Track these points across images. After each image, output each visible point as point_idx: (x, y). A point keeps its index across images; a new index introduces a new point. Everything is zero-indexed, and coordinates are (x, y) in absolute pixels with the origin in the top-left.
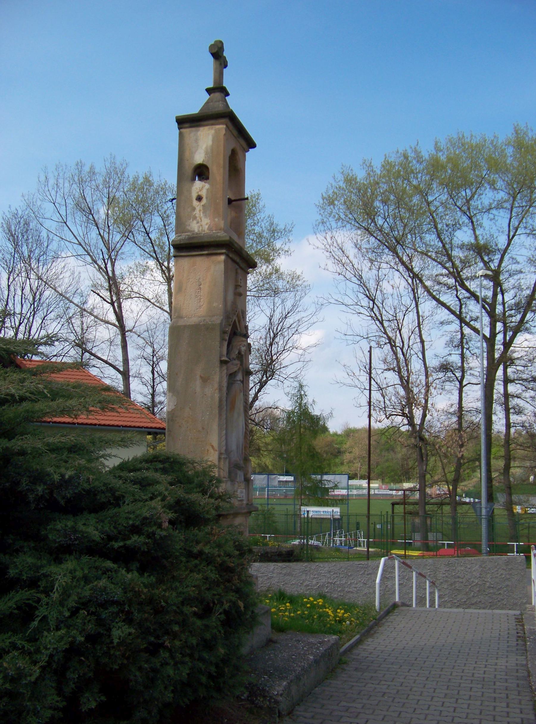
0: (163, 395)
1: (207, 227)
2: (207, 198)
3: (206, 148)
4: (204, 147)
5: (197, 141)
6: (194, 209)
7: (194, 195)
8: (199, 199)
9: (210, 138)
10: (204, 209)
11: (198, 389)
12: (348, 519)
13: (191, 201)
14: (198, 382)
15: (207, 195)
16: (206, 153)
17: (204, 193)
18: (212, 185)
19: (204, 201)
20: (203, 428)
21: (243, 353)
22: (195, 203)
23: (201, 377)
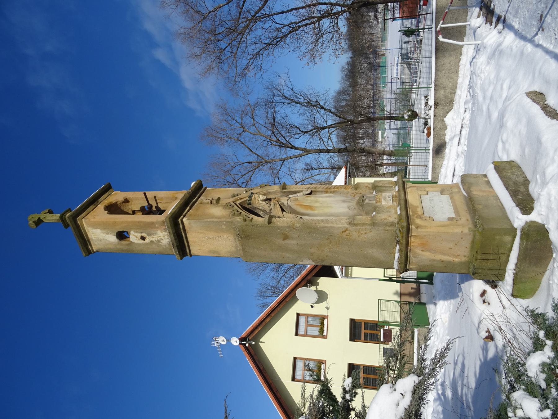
0: (361, 164)
1: (164, 233)
2: (142, 233)
3: (104, 233)
4: (104, 235)
5: (100, 240)
6: (152, 241)
7: (142, 242)
8: (143, 238)
9: (95, 230)
10: (151, 235)
11: (294, 242)
12: (405, 294)
13: (147, 244)
14: (287, 242)
15: (139, 233)
16: (107, 233)
17: (139, 235)
18: (131, 229)
19: (144, 235)
20: (328, 239)
21: (265, 198)
22: (148, 240)
23: (284, 240)
